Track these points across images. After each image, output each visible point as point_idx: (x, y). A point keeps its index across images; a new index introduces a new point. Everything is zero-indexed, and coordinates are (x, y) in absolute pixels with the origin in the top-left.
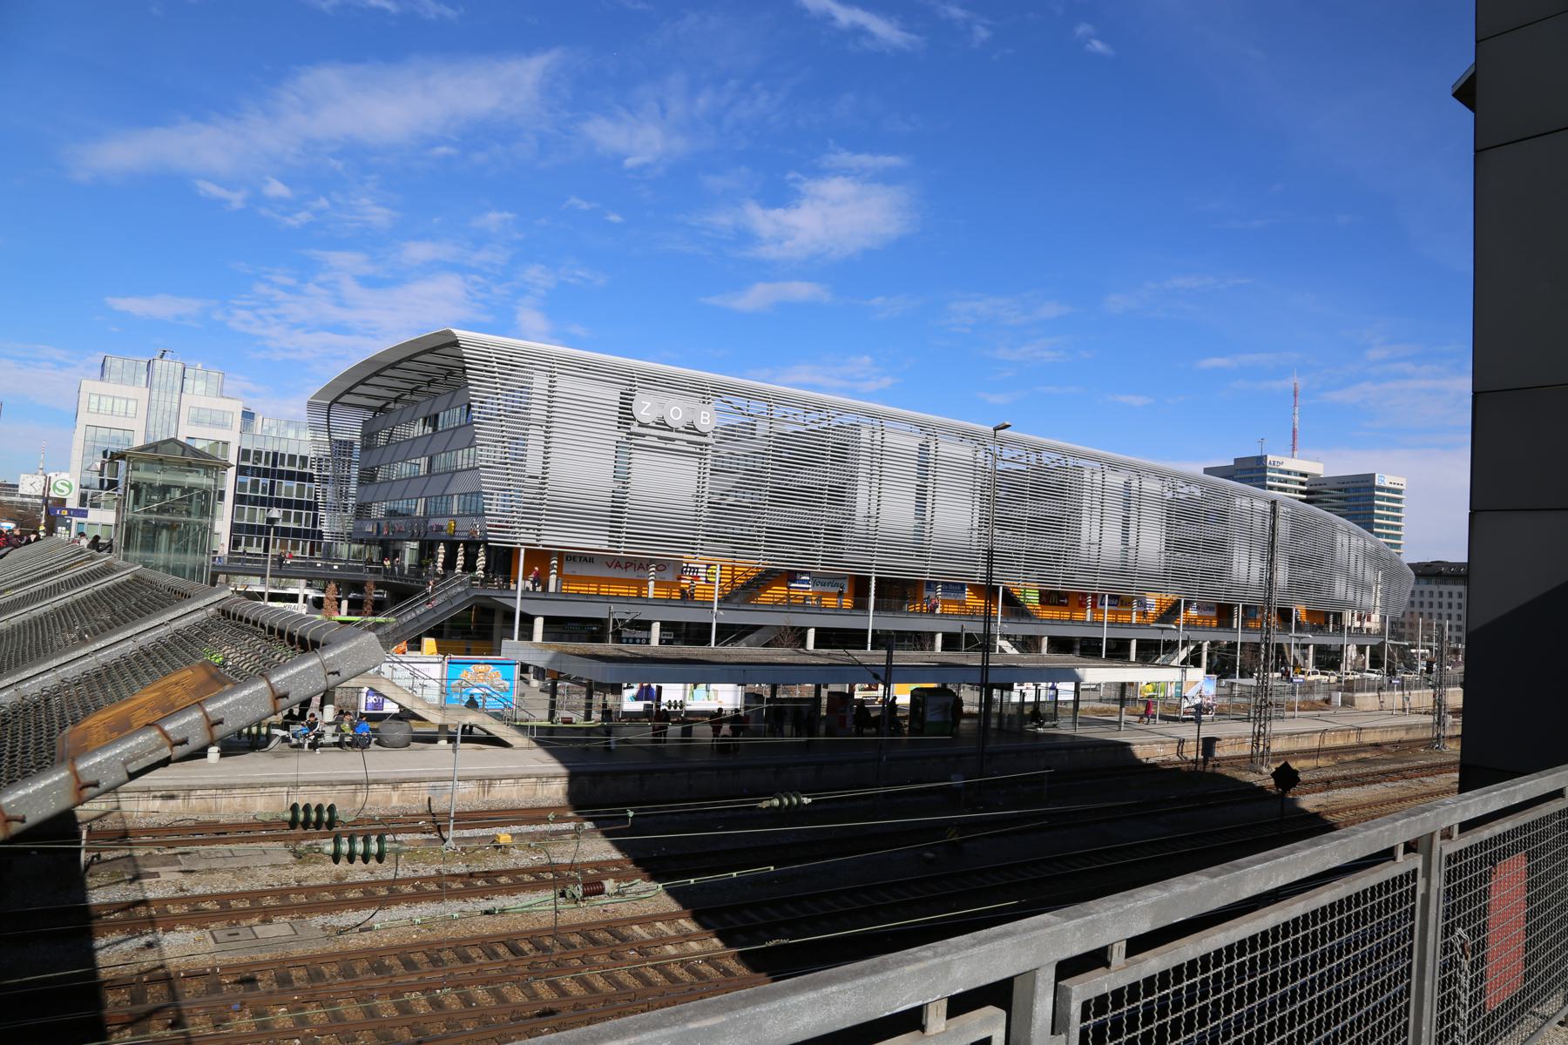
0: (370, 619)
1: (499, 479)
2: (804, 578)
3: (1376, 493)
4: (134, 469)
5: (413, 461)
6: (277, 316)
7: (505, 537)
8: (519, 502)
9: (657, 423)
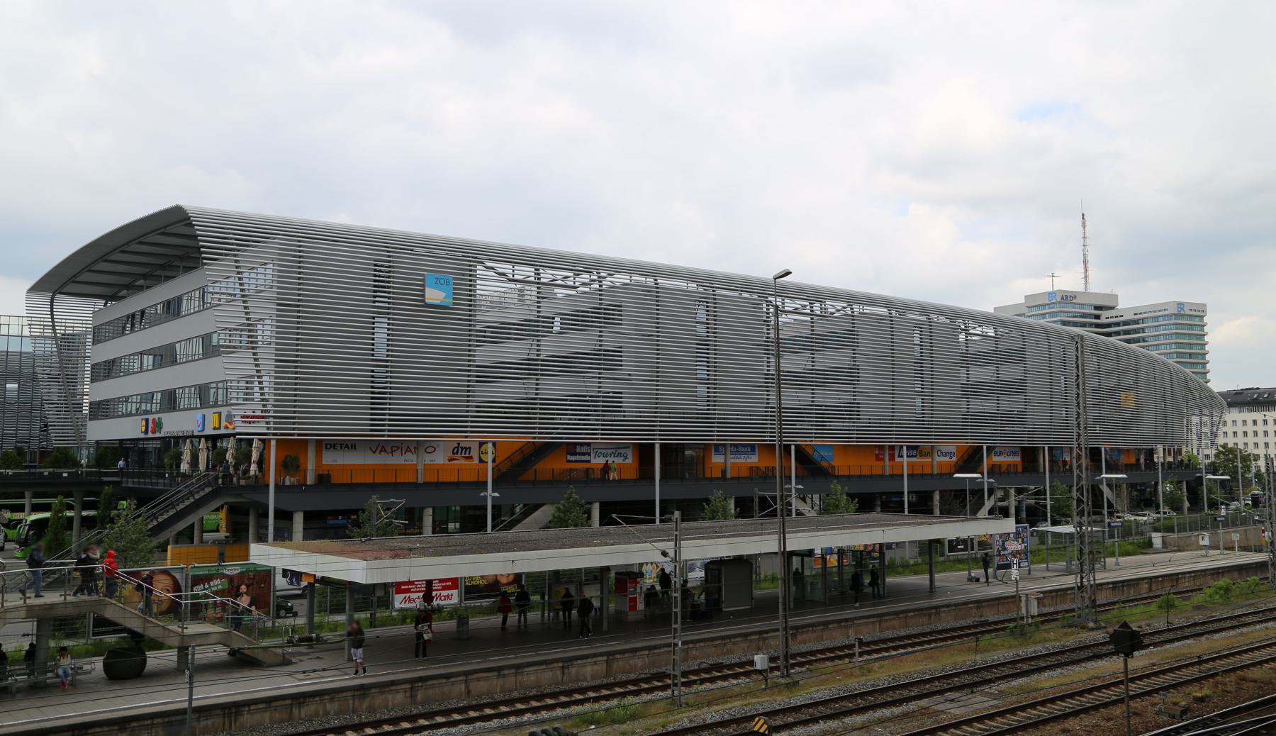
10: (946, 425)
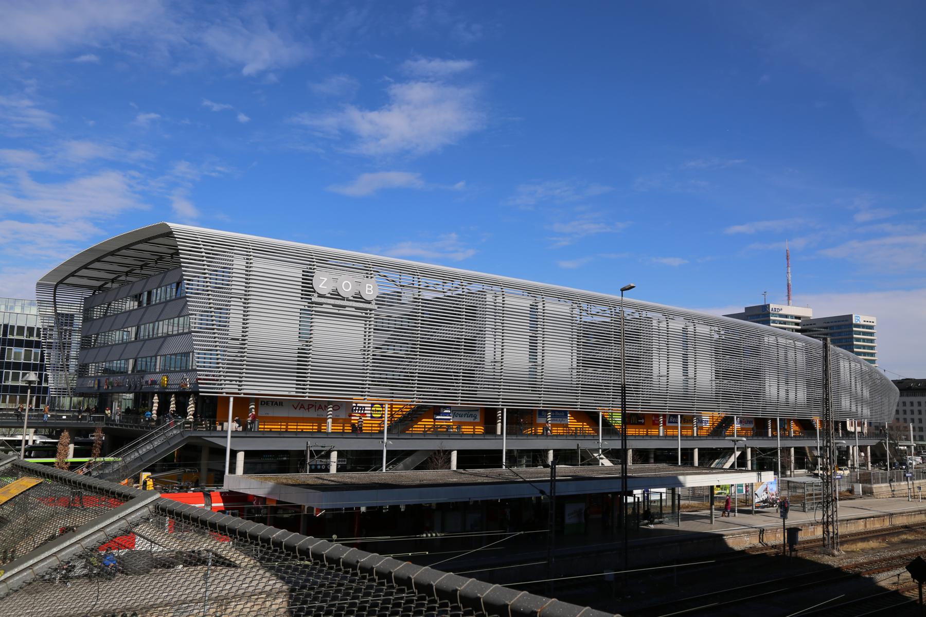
1: (196, 306)
3: (854, 329)
5: (126, 330)
9: (331, 294)
10: (557, 392)
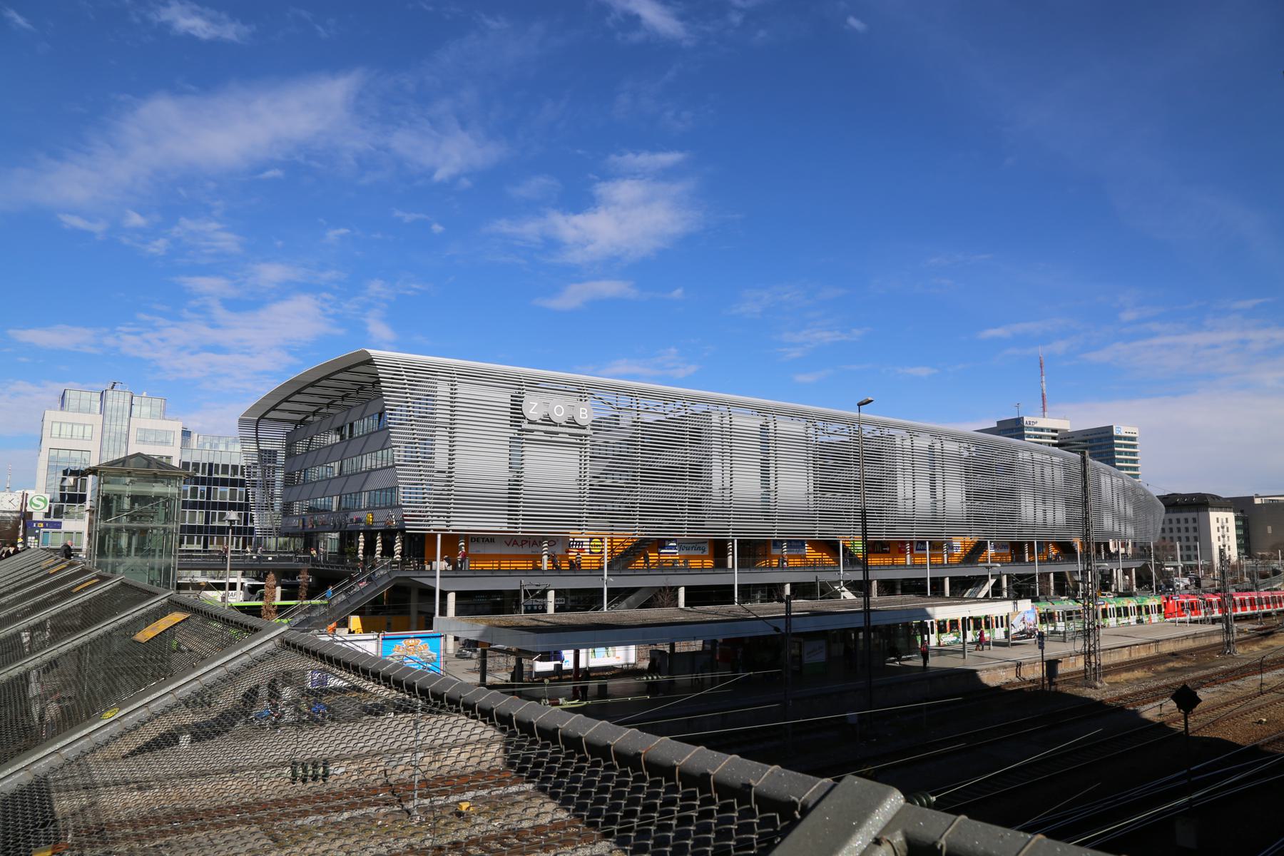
0: (305, 602)
2: (671, 544)
3: (1115, 441)
4: (105, 483)
5: (328, 465)
6: (162, 340)
7: (419, 525)
8: (429, 494)
9: (543, 420)
